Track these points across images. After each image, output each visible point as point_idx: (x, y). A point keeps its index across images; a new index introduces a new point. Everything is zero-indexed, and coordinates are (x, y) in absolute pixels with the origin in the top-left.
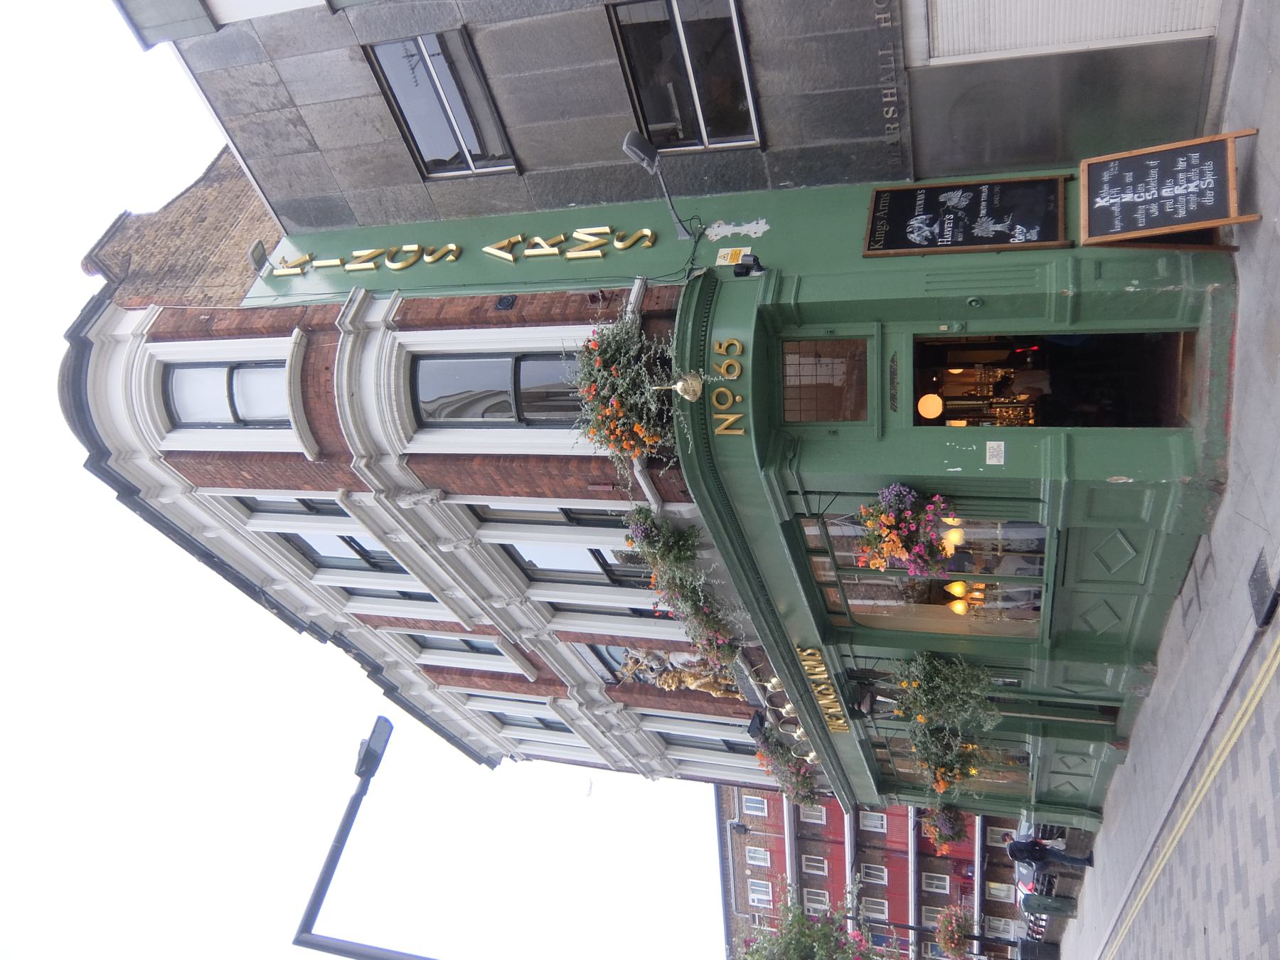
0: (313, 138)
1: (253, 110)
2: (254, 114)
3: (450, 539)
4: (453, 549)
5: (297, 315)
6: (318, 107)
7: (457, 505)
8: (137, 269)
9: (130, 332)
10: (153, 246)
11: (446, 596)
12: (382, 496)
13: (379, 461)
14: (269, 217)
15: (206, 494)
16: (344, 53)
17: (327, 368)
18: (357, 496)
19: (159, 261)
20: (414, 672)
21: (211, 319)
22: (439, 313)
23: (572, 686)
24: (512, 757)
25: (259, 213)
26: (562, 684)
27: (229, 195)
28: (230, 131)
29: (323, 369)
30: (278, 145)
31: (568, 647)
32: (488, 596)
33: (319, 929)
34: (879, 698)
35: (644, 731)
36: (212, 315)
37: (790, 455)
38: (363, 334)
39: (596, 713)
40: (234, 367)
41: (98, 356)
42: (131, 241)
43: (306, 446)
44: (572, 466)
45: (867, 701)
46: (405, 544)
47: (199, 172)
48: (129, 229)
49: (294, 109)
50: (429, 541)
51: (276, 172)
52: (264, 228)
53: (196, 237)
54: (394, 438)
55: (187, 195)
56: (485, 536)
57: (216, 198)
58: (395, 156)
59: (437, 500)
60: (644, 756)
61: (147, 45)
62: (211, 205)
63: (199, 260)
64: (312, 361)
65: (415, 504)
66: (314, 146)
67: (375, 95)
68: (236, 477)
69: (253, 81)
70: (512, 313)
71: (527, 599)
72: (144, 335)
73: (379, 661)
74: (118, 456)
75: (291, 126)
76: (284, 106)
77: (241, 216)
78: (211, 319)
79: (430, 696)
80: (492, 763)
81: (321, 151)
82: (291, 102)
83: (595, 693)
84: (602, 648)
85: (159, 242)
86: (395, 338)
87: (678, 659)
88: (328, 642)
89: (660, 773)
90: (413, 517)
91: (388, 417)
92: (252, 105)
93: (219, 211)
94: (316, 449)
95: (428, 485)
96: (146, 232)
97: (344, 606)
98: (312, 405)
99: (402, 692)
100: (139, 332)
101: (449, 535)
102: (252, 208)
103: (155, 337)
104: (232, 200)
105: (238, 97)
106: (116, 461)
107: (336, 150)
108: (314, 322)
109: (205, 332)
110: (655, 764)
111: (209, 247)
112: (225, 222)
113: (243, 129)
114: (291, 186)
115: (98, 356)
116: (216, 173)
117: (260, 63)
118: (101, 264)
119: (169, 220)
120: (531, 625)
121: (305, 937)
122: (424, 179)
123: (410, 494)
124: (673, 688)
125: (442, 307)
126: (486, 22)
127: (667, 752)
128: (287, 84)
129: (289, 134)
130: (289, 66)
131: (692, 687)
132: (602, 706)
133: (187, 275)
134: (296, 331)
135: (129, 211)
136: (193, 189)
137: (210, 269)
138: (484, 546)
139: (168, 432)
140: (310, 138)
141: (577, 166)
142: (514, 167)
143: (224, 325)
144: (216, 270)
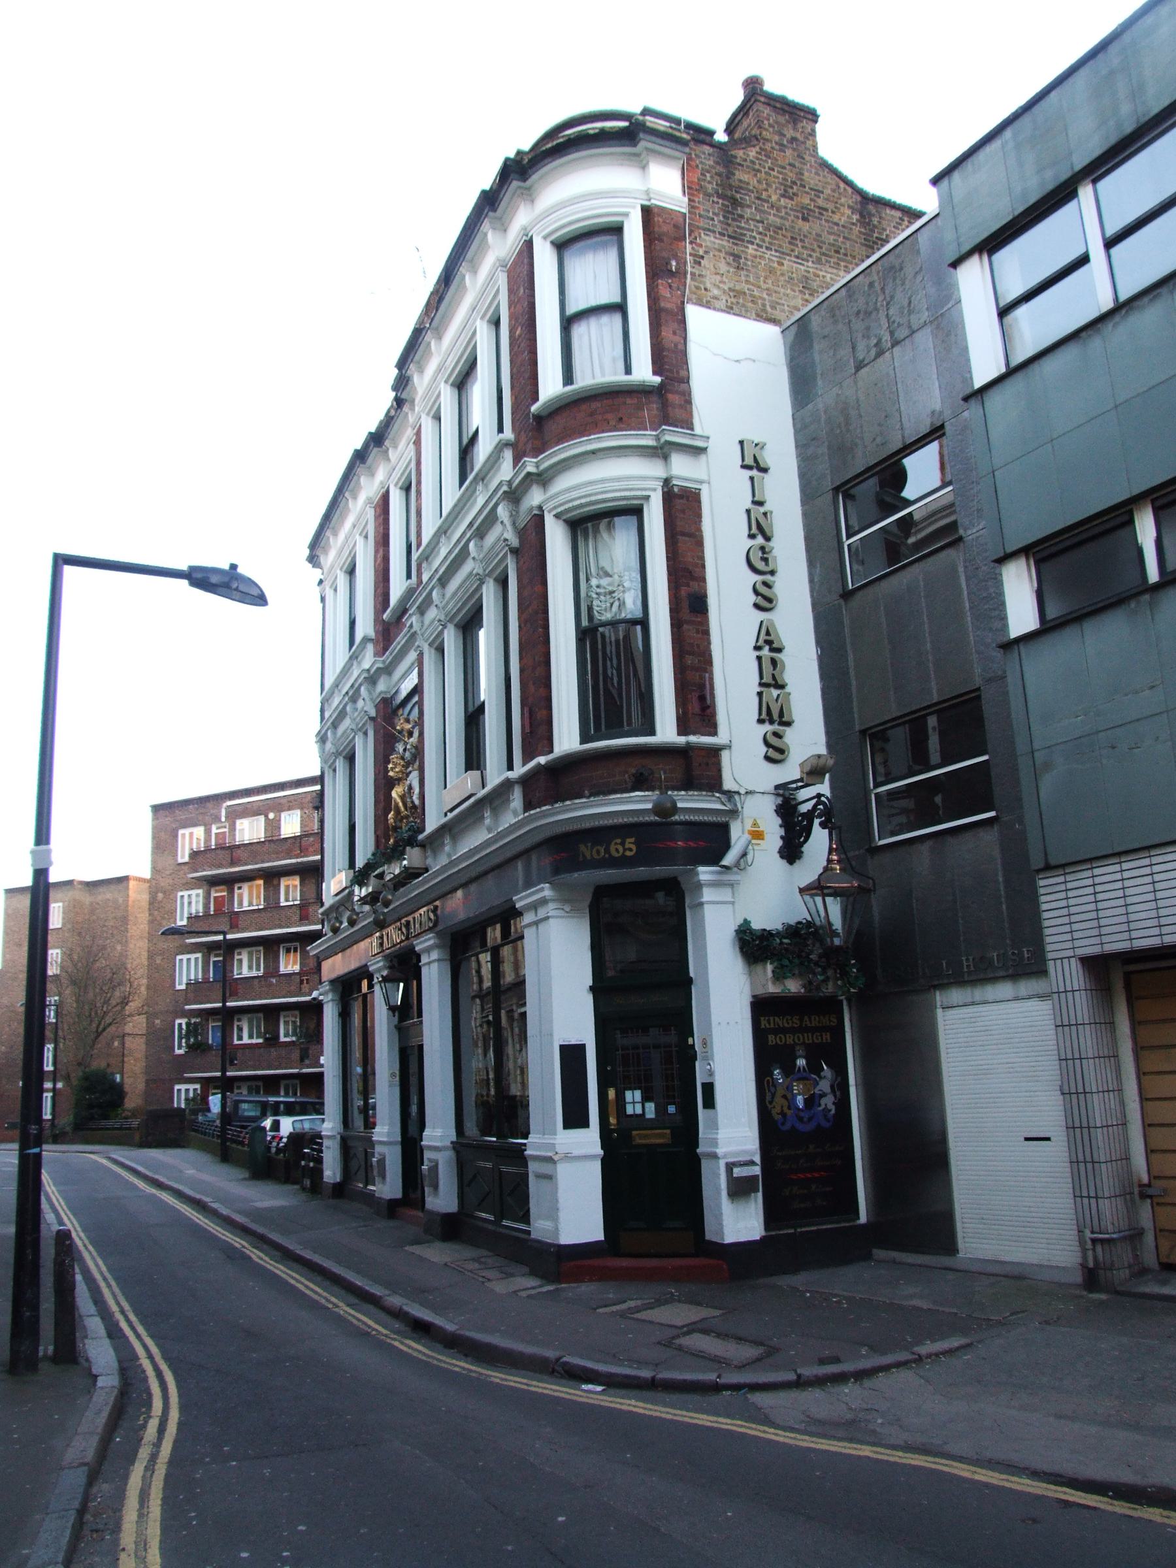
0: (866, 365)
1: (888, 299)
2: (885, 299)
3: (482, 550)
4: (472, 555)
5: (678, 372)
6: (892, 372)
7: (507, 565)
8: (738, 161)
9: (650, 186)
10: (769, 168)
11: (440, 536)
12: (505, 488)
13: (538, 483)
14: (809, 298)
15: (500, 282)
16: (937, 405)
17: (621, 419)
18: (508, 455)
19: (748, 184)
20: (382, 483)
21: (671, 274)
22: (683, 534)
23: (384, 662)
24: (321, 582)
25: (815, 285)
26: (385, 649)
27: (841, 239)
28: (869, 270)
29: (620, 415)
30: (858, 325)
31: (413, 664)
32: (443, 582)
33: (68, 569)
34: (402, 985)
35: (354, 737)
36: (681, 274)
37: (567, 908)
38: (661, 452)
39: (362, 688)
40: (620, 308)
41: (624, 154)
42: (777, 138)
43: (545, 403)
44: (542, 690)
45: (398, 975)
46: (476, 500)
47: (873, 188)
48: (795, 129)
49: (889, 345)
50: (478, 529)
51: (836, 322)
52: (794, 297)
53: (782, 218)
54: (562, 499)
55: (842, 185)
56: (488, 588)
57: (837, 224)
58: (853, 457)
59: (507, 545)
60: (334, 734)
61: (936, 181)
62: (826, 221)
63: (749, 233)
64: (629, 401)
65: (502, 522)
66: (859, 366)
67: (903, 437)
68: (517, 319)
69: (913, 298)
70: (686, 614)
71: (445, 626)
72: (650, 200)
73: (387, 443)
74: (526, 189)
75: (875, 341)
76: (892, 333)
77: (810, 264)
78: (671, 274)
79: (362, 497)
80: (313, 559)
81: (855, 374)
82: (896, 343)
83: (382, 686)
84: (416, 699)
85: (775, 173)
86: (655, 490)
87: (414, 778)
88: (394, 394)
89: (322, 750)
90: (491, 518)
91: (575, 494)
92: (892, 297)
93: (817, 235)
94: (544, 414)
95: (521, 533)
96: (789, 152)
97: (428, 414)
98: (584, 407)
99: (361, 469)
100: (652, 196)
101: (448, 595)
102: (821, 273)
103: (648, 213)
104: (833, 245)
105: (898, 282)
106: (520, 187)
107: (856, 391)
108: (670, 396)
109: (656, 270)
110: (329, 745)
111: (767, 239)
112: (803, 247)
113: (871, 285)
114: (825, 337)
115: (624, 154)
116: (874, 211)
117: (927, 309)
118: (748, 106)
119: (806, 174)
120: (425, 627)
121: (61, 561)
122: (836, 490)
123: (511, 515)
124: (391, 774)
125: (691, 535)
126: (965, 561)
127: (341, 758)
128: (910, 338)
129: (868, 338)
130: (925, 340)
131: (394, 794)
132: (370, 693)
133: (729, 225)
134: (657, 379)
135: (820, 119)
136: (850, 190)
137: (737, 250)
138: (479, 588)
139: (552, 243)
140: (866, 362)
141: (851, 658)
142: (850, 587)
143: (664, 292)
144: (737, 257)
